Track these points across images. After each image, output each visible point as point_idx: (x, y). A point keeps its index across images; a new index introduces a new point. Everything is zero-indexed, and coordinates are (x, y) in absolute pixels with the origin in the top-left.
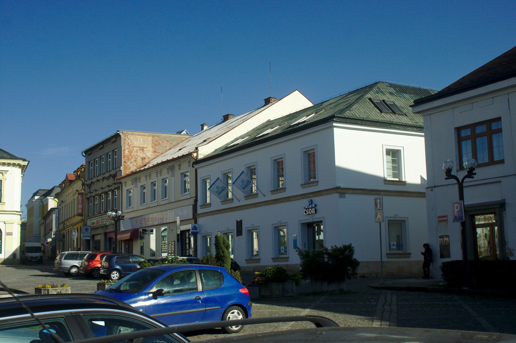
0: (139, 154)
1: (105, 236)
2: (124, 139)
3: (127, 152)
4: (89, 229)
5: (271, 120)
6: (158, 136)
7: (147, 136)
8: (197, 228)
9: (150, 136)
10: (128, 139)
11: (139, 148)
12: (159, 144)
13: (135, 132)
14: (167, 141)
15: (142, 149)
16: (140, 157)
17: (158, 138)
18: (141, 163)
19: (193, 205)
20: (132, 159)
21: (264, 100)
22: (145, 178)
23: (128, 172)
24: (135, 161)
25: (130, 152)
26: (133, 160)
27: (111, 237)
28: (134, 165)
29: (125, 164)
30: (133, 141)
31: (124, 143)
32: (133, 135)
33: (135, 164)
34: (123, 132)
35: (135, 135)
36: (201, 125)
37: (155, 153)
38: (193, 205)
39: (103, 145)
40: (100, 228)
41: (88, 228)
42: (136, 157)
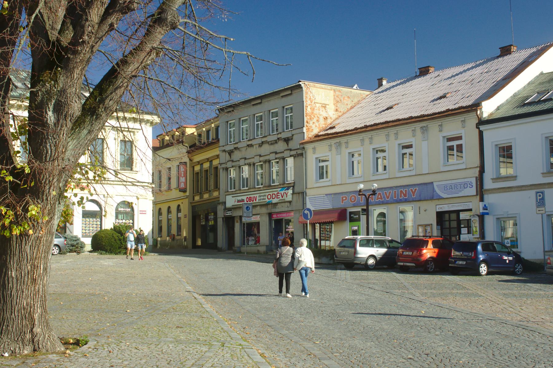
0: (321, 113)
1: (269, 216)
2: (306, 92)
3: (309, 109)
4: (251, 207)
5: (544, 72)
6: (340, 91)
7: (329, 90)
8: (487, 207)
9: (331, 90)
10: (309, 93)
11: (321, 105)
12: (341, 101)
13: (311, 83)
14: (348, 97)
15: (324, 106)
16: (323, 116)
17: (340, 93)
18: (323, 124)
19: (476, 177)
20: (315, 118)
21: (500, 48)
22: (360, 143)
23: (311, 135)
24: (318, 121)
25: (313, 109)
26: (315, 120)
27: (282, 219)
28: (316, 126)
29: (307, 124)
30: (315, 96)
31: (306, 97)
32: (315, 87)
33: (318, 126)
34: (305, 83)
35: (317, 87)
36: (378, 79)
37: (337, 113)
38: (476, 177)
39: (261, 99)
40: (258, 207)
41: (249, 206)
42: (319, 116)
